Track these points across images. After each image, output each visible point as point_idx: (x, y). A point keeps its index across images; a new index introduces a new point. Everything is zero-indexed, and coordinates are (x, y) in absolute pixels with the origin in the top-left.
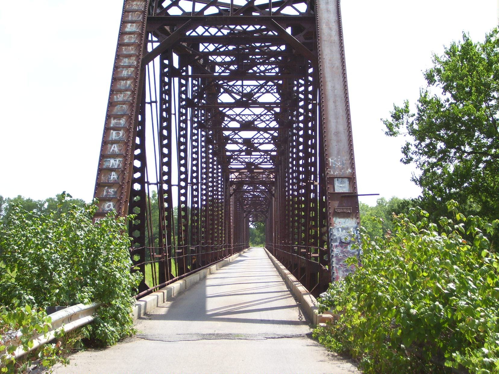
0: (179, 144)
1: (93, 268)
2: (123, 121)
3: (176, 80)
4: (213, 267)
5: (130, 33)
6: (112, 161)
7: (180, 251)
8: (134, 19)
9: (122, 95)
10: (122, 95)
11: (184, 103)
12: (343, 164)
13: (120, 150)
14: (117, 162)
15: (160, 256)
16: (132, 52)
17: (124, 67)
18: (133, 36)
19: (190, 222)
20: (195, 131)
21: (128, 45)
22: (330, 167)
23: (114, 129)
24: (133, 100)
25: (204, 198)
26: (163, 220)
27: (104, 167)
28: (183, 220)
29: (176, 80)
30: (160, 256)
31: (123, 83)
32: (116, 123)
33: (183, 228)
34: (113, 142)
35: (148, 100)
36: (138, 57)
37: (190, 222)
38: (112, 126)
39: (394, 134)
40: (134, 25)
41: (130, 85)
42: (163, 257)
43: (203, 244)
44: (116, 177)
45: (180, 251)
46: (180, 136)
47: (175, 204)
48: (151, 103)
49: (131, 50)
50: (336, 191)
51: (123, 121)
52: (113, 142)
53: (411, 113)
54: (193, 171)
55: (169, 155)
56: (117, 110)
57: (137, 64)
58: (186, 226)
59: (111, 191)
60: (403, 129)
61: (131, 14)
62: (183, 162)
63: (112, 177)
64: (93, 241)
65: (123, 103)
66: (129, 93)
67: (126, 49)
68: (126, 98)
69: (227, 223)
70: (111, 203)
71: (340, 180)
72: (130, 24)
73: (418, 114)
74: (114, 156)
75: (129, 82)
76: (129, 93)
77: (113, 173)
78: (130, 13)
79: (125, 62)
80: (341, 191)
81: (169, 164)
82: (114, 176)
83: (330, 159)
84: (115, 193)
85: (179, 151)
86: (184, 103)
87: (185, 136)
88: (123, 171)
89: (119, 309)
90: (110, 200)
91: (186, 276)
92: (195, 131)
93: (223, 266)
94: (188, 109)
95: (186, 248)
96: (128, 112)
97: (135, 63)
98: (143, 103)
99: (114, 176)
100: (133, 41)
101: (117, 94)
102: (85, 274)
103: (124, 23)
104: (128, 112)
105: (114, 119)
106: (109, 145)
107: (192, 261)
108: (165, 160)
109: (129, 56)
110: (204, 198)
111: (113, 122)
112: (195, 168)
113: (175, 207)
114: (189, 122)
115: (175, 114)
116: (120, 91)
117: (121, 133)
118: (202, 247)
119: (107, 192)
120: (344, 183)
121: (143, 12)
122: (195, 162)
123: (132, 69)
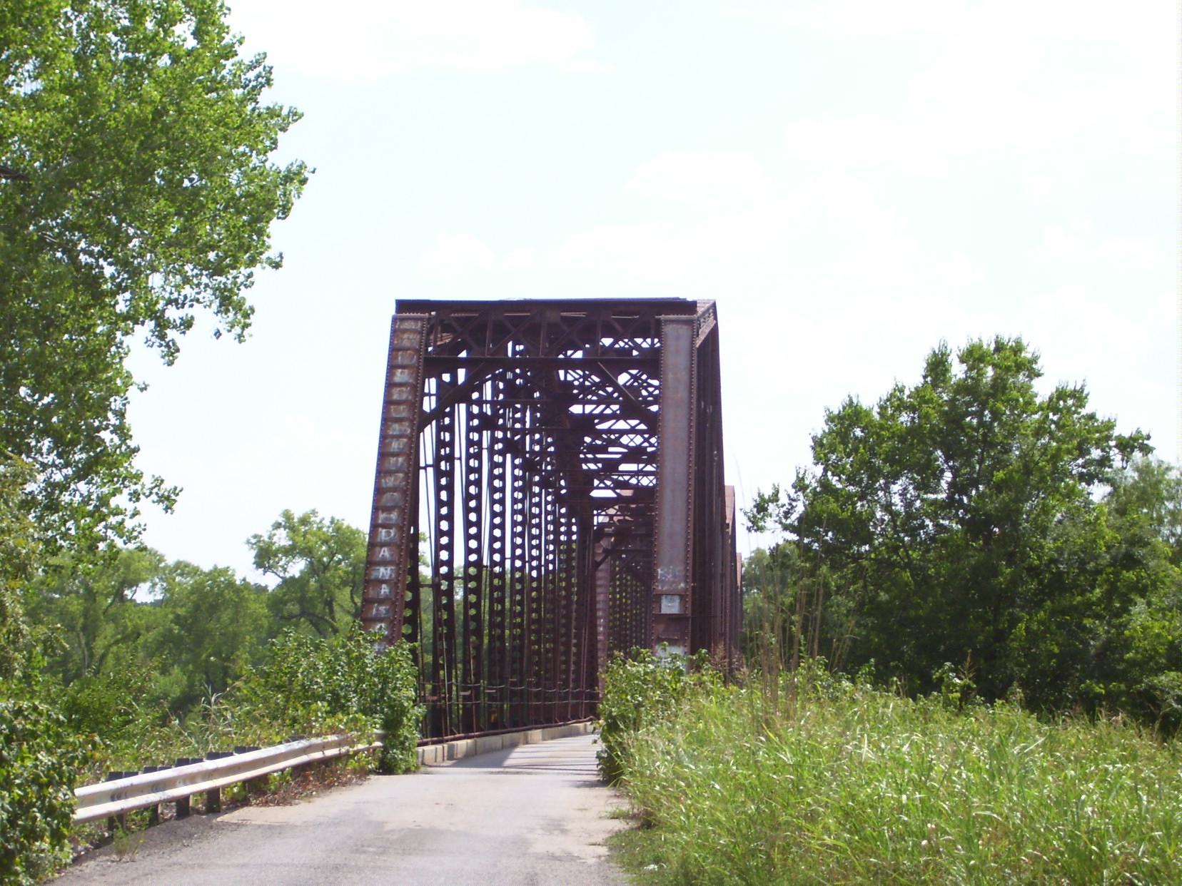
0: (467, 497)
1: (382, 697)
2: (394, 516)
3: (463, 407)
4: (536, 734)
5: (401, 385)
6: (382, 570)
7: (468, 693)
8: (406, 362)
9: (392, 479)
10: (392, 479)
11: (476, 422)
12: (674, 576)
13: (392, 555)
14: (389, 571)
15: (435, 698)
16: (404, 415)
17: (393, 437)
18: (404, 389)
19: (486, 640)
20: (498, 459)
21: (399, 403)
22: (658, 581)
23: (384, 526)
24: (406, 485)
25: (551, 547)
26: (441, 639)
27: (373, 577)
28: (473, 638)
29: (463, 407)
30: (435, 698)
31: (393, 460)
32: (386, 519)
33: (472, 652)
34: (383, 545)
35: (422, 464)
36: (412, 421)
37: (486, 640)
38: (380, 522)
39: (760, 529)
40: (406, 371)
41: (402, 464)
42: (439, 700)
43: (514, 684)
44: (387, 590)
45: (468, 693)
46: (469, 483)
47: (459, 562)
48: (425, 468)
49: (403, 412)
50: (663, 612)
51: (394, 516)
52: (383, 545)
53: (780, 503)
54: (493, 539)
55: (450, 533)
56: (387, 498)
57: (411, 433)
58: (478, 647)
59: (382, 608)
60: (769, 523)
61: (402, 356)
62: (473, 531)
63: (383, 591)
64: (382, 669)
65: (394, 489)
66: (401, 475)
67: (395, 410)
68: (397, 483)
69: (585, 635)
70: (383, 625)
71: (669, 597)
72: (400, 370)
73: (790, 504)
74: (384, 563)
75: (400, 459)
76: (401, 475)
77: (384, 586)
78: (400, 353)
79: (394, 430)
80: (668, 611)
81: (450, 518)
82: (385, 589)
83: (659, 570)
84: (387, 611)
85: (467, 510)
86: (476, 422)
87: (478, 483)
88: (396, 584)
89: (406, 738)
90: (381, 620)
91: (478, 736)
92: (498, 459)
93: (564, 736)
94: (485, 432)
95: (477, 689)
96: (401, 504)
97: (409, 431)
98: (417, 468)
99: (385, 589)
100: (404, 397)
101: (385, 477)
102: (375, 701)
103: (392, 368)
104: (401, 504)
105: (383, 512)
106: (377, 549)
107: (490, 718)
108: (444, 540)
109: (399, 420)
110: (551, 547)
111: (382, 516)
112: (497, 533)
113: (459, 568)
114: (485, 454)
115: (460, 459)
116: (390, 473)
117: (393, 532)
118: (512, 691)
119: (377, 610)
120: (674, 601)
121: (418, 351)
122: (497, 521)
123: (405, 440)
